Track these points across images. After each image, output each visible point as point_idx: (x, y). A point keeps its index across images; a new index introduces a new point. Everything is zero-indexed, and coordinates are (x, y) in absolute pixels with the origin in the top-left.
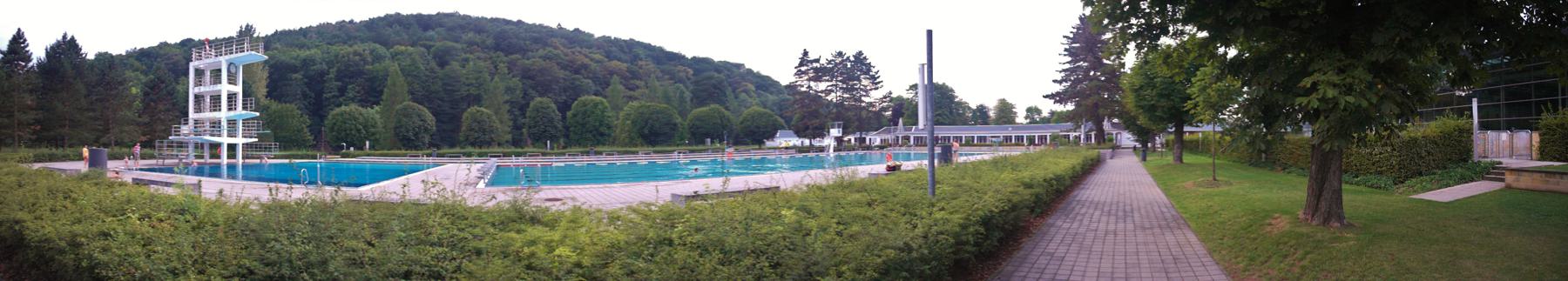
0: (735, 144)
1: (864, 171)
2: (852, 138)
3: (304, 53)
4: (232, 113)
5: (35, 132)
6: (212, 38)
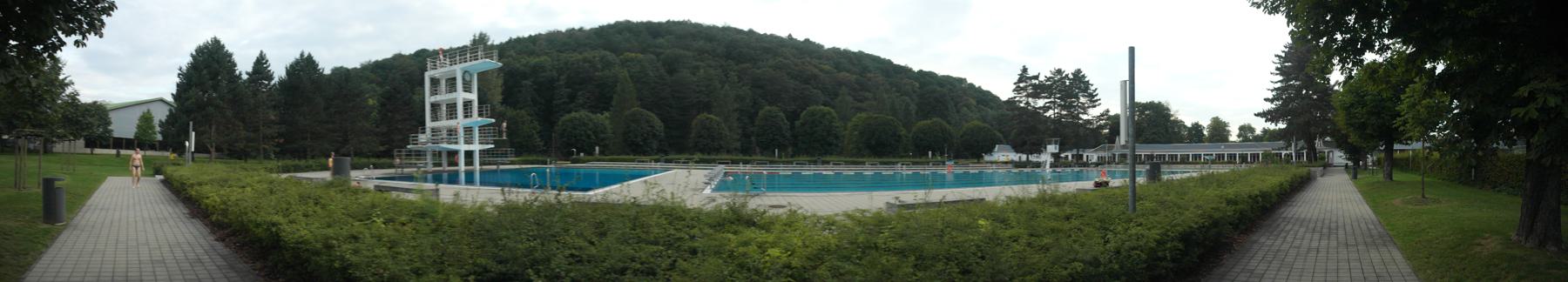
0: (956, 157)
1: (1069, 187)
2: (1070, 155)
3: (534, 61)
4: (468, 121)
5: (278, 145)
6: (446, 47)
